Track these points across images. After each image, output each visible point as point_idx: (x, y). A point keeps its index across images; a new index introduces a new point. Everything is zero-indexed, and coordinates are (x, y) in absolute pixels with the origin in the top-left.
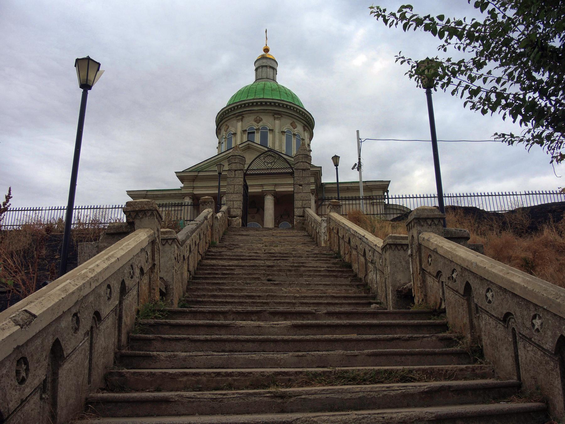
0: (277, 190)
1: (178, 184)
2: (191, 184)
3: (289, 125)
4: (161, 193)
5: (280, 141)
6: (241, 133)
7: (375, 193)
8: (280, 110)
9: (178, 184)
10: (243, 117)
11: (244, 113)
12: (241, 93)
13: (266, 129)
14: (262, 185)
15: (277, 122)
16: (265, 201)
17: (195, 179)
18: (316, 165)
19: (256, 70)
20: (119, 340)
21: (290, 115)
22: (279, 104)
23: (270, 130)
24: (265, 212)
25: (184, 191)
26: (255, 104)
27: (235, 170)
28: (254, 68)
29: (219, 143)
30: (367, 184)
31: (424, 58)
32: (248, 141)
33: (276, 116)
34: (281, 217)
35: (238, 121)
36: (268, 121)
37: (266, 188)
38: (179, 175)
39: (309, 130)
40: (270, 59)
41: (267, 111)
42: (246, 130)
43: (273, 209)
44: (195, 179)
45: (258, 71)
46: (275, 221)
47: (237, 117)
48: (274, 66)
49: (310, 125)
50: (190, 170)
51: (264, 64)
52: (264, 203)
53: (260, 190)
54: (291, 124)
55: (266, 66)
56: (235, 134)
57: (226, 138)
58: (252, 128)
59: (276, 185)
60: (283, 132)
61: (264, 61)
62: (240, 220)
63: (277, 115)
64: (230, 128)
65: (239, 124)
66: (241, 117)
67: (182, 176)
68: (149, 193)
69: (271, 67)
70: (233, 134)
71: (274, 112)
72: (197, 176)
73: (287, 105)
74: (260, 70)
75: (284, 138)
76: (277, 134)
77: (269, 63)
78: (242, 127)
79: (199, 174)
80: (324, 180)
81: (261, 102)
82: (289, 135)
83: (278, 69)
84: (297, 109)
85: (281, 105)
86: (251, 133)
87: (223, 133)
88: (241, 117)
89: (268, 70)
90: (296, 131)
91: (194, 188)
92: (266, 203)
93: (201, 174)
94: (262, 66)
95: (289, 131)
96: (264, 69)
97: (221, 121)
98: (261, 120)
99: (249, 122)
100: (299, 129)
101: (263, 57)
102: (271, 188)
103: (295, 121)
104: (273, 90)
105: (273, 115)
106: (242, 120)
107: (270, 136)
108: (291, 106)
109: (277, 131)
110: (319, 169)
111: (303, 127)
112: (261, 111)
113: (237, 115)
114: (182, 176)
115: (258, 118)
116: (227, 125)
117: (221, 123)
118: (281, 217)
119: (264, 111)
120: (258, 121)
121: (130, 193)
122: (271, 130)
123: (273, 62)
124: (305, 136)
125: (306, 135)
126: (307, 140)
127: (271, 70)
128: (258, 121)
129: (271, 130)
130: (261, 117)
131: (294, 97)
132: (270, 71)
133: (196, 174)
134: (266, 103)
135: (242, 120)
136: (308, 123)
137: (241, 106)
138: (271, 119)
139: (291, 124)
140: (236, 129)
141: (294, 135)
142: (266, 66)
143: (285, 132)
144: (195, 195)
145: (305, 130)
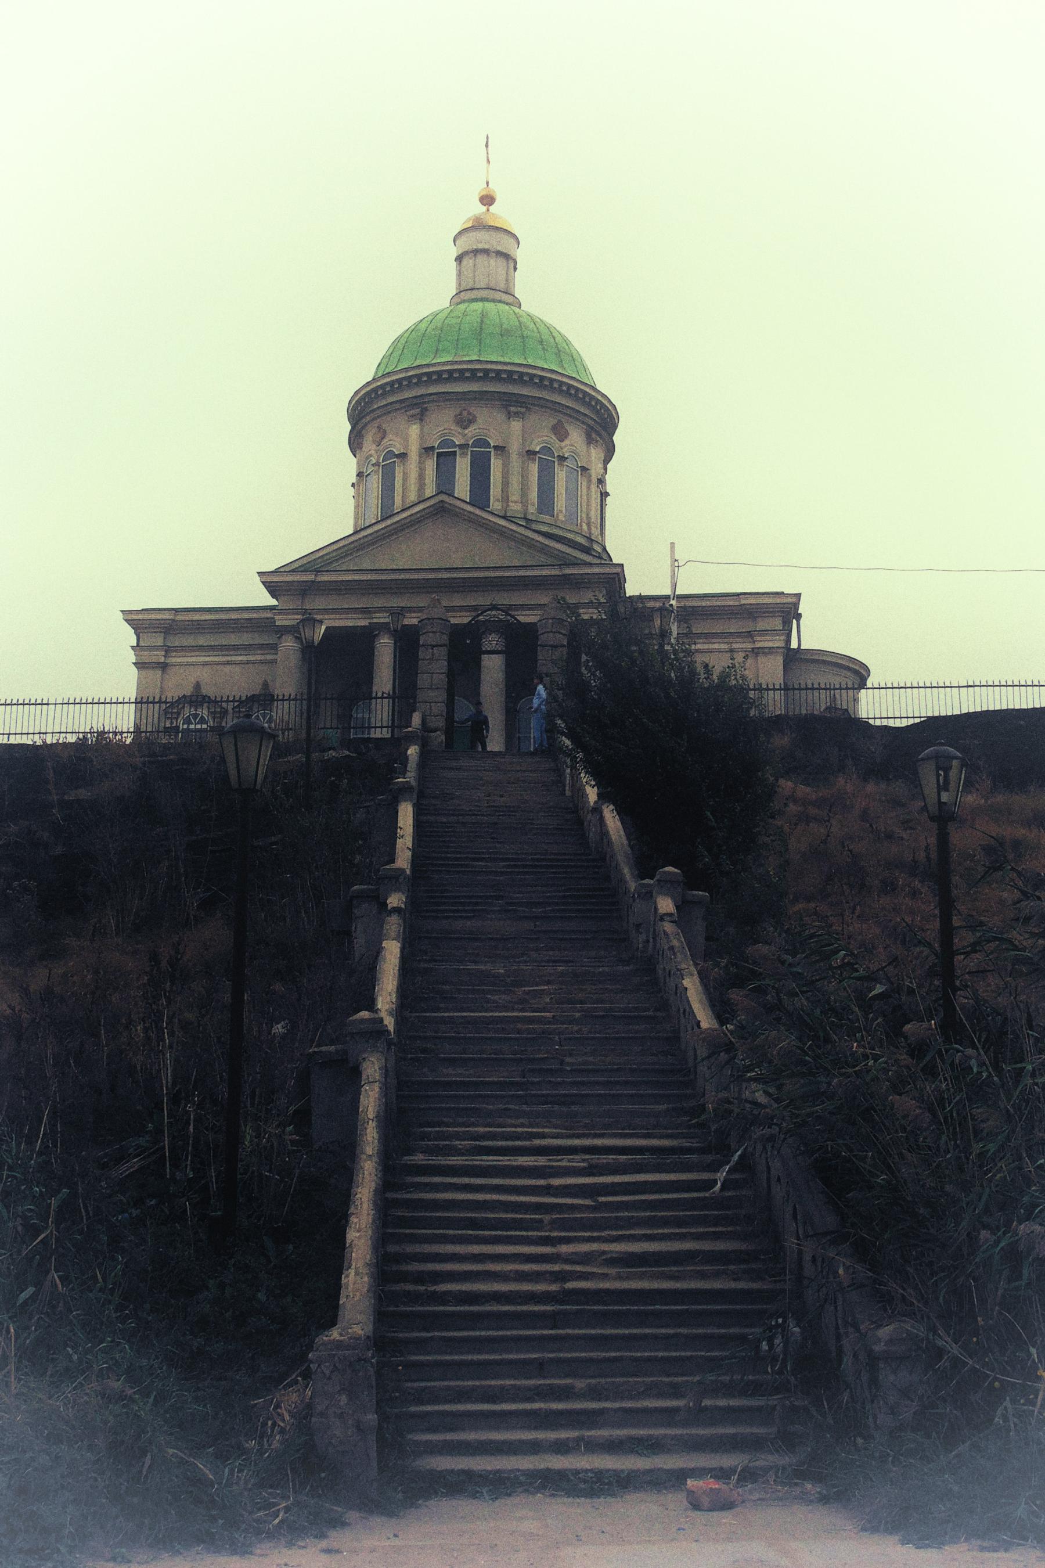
1: (267, 600)
4: (212, 617)
5: (524, 476)
6: (420, 456)
9: (267, 600)
10: (426, 409)
13: (488, 445)
15: (516, 425)
19: (459, 259)
23: (496, 448)
25: (281, 621)
27: (434, 646)
28: (454, 252)
29: (359, 475)
31: (637, 594)
32: (442, 492)
33: (512, 409)
36: (490, 424)
39: (604, 440)
42: (432, 448)
44: (305, 590)
45: (465, 262)
46: (508, 696)
49: (605, 429)
50: (296, 565)
51: (480, 246)
55: (486, 251)
56: (403, 456)
57: (377, 464)
60: (531, 453)
62: (443, 737)
63: (514, 406)
65: (414, 430)
66: (419, 409)
67: (273, 583)
68: (180, 617)
69: (499, 254)
70: (399, 456)
74: (468, 262)
76: (514, 456)
78: (422, 437)
79: (319, 579)
83: (521, 255)
84: (570, 386)
86: (445, 459)
87: (369, 445)
89: (492, 262)
90: (565, 448)
93: (325, 578)
94: (476, 252)
96: (481, 259)
99: (441, 425)
100: (576, 437)
101: (478, 225)
104: (505, 333)
105: (506, 407)
106: (421, 417)
107: (496, 465)
110: (618, 570)
114: (273, 583)
115: (465, 413)
120: (464, 422)
126: (596, 469)
127: (501, 262)
131: (561, 349)
132: (496, 265)
133: (311, 577)
134: (486, 372)
138: (500, 416)
140: (406, 439)
141: (562, 459)
142: (486, 252)
143: (535, 453)
145: (590, 440)
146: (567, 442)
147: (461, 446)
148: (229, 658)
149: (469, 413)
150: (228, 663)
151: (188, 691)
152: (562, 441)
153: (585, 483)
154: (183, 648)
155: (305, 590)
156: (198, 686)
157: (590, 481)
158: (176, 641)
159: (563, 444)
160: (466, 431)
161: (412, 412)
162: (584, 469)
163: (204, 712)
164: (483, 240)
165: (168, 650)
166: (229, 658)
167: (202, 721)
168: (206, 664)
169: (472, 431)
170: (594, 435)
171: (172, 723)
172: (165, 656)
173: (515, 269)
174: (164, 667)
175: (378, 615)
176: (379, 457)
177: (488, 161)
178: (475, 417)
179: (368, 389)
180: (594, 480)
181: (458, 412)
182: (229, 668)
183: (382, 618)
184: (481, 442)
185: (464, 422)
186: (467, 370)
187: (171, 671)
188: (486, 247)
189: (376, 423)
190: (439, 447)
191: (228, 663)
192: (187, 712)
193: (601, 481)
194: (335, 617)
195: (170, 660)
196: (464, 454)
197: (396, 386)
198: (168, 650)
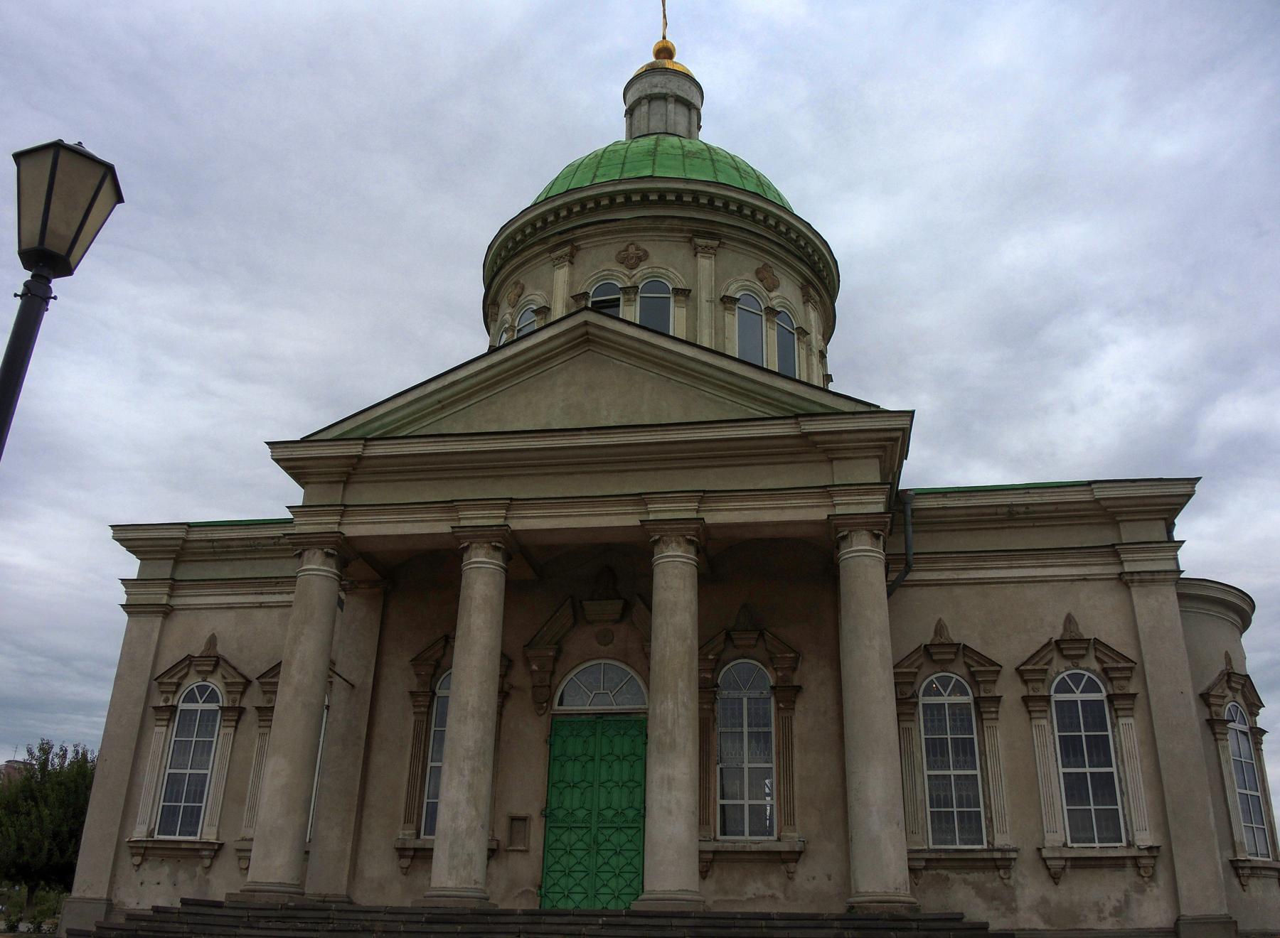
0: (711, 518)
2: (335, 495)
3: (749, 275)
7: (1130, 533)
8: (718, 219)
10: (578, 249)
11: (579, 233)
12: (574, 169)
14: (641, 499)
15: (705, 264)
16: (657, 571)
19: (630, 113)
21: (752, 239)
22: (712, 198)
23: (677, 292)
24: (657, 620)
25: (308, 526)
26: (620, 199)
30: (1099, 494)
33: (700, 241)
34: (728, 637)
35: (557, 263)
36: (668, 261)
37: (660, 511)
38: (286, 453)
39: (823, 303)
41: (667, 224)
42: (585, 295)
43: (694, 607)
45: (637, 113)
46: (702, 658)
47: (552, 250)
48: (696, 101)
51: (656, 91)
52: (649, 576)
53: (634, 521)
58: (611, 288)
59: (704, 496)
60: (728, 302)
61: (658, 79)
64: (527, 292)
65: (561, 276)
67: (294, 458)
69: (680, 100)
71: (694, 226)
72: (360, 458)
73: (741, 205)
77: (674, 86)
78: (571, 285)
81: (644, 194)
85: (719, 203)
88: (567, 249)
91: (344, 510)
92: (659, 580)
94: (651, 98)
98: (642, 257)
99: (599, 266)
100: (787, 293)
101: (650, 70)
102: (684, 510)
103: (770, 261)
104: (686, 155)
105: (690, 240)
106: (571, 259)
108: (755, 210)
111: (803, 288)
112: (644, 224)
114: (294, 458)
115: (632, 249)
116: (517, 283)
117: (498, 280)
118: (728, 637)
120: (632, 260)
121: (128, 536)
122: (683, 294)
123: (683, 81)
124: (807, 320)
125: (813, 319)
126: (816, 337)
127: (682, 110)
128: (632, 260)
129: (683, 294)
130: (644, 246)
132: (678, 116)
133: (355, 449)
134: (662, 194)
135: (571, 259)
137: (570, 211)
138: (680, 254)
139: (758, 272)
140: (550, 293)
141: (771, 312)
142: (663, 97)
144: (349, 540)
145: (807, 299)
147: (625, 290)
149: (638, 249)
151: (197, 649)
153: (803, 353)
155: (349, 474)
156: (212, 641)
159: (773, 294)
163: (215, 683)
164: (659, 84)
165: (174, 585)
167: (213, 697)
168: (230, 607)
169: (642, 270)
170: (812, 291)
171: (166, 700)
172: (170, 596)
173: (699, 128)
174: (167, 612)
178: (646, 254)
180: (816, 351)
182: (260, 614)
184: (655, 284)
186: (636, 191)
187: (180, 624)
190: (596, 294)
191: (261, 606)
192: (193, 682)
193: (823, 355)
195: (177, 602)
196: (629, 302)
198: (174, 585)
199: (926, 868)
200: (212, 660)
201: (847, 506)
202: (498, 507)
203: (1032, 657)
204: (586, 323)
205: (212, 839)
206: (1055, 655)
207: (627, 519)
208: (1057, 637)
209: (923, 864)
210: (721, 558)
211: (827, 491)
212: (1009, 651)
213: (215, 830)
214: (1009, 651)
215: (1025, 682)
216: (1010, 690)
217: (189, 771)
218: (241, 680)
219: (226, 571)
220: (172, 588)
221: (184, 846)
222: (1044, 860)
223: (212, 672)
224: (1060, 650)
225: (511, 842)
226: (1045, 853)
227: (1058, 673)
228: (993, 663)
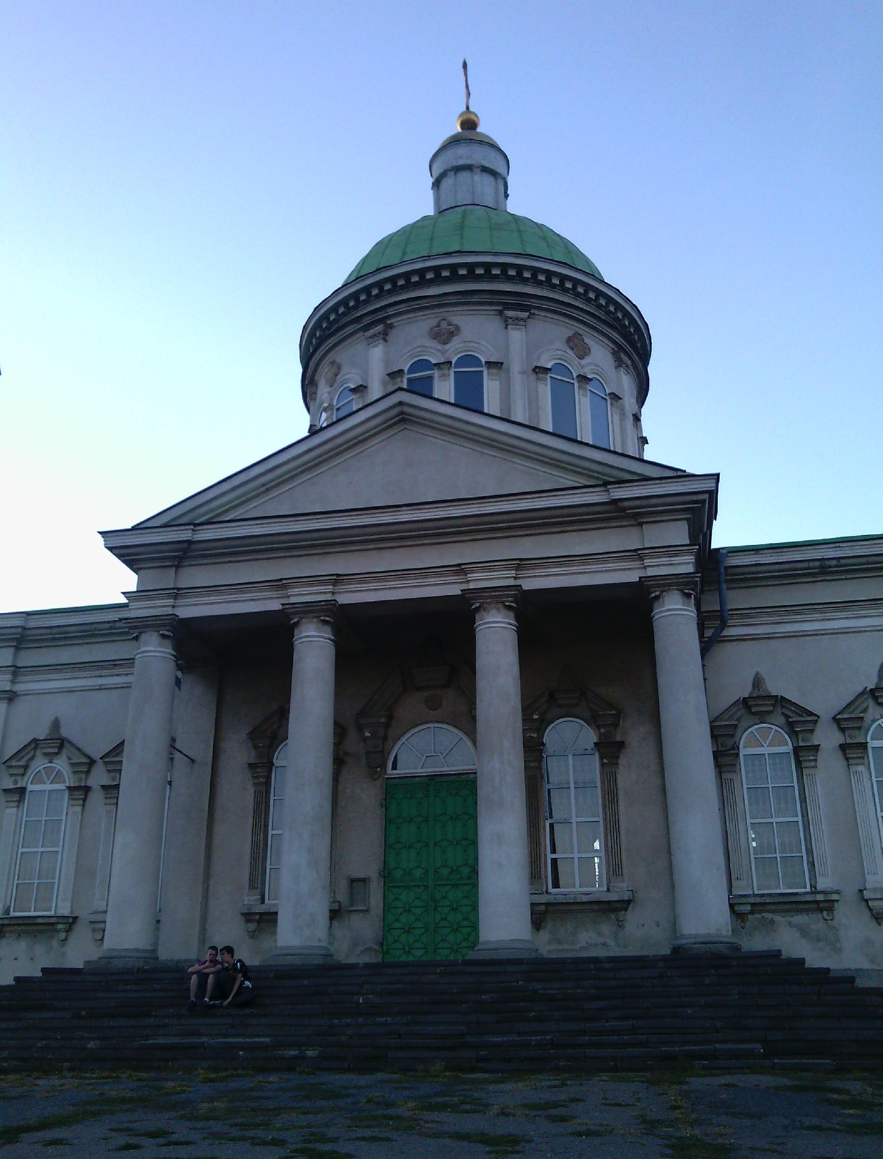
1: (111, 583)
2: (167, 579)
3: (561, 344)
10: (391, 326)
11: (391, 311)
15: (516, 336)
16: (479, 636)
17: (182, 555)
18: (690, 470)
19: (437, 184)
20: (633, 525)
23: (489, 364)
28: (430, 181)
33: (510, 313)
37: (479, 580)
38: (117, 542)
40: (481, 142)
42: (400, 372)
44: (182, 555)
46: (527, 711)
48: (501, 170)
51: (461, 162)
54: (569, 340)
60: (540, 371)
67: (126, 546)
68: (32, 624)
69: (485, 170)
70: (354, 390)
72: (189, 542)
75: (545, 391)
78: (387, 362)
80: (723, 536)
82: (565, 385)
83: (512, 180)
87: (323, 390)
88: (380, 328)
90: (587, 367)
94: (458, 169)
95: (561, 368)
96: (464, 176)
97: (316, 349)
99: (412, 340)
100: (600, 357)
103: (581, 329)
105: (501, 313)
109: (516, 366)
110: (709, 485)
111: (614, 354)
112: (453, 299)
113: (366, 321)
115: (444, 325)
116: (333, 363)
119: (465, 299)
120: (444, 335)
125: (626, 384)
127: (488, 179)
130: (456, 320)
132: (485, 186)
133: (186, 535)
136: (629, 338)
141: (583, 379)
142: (469, 168)
143: (547, 370)
145: (619, 363)
146: (586, 360)
148: (101, 681)
149: (450, 324)
150: (101, 688)
152: (581, 357)
153: (617, 418)
154: (36, 669)
156: (56, 725)
157: (623, 415)
158: (29, 658)
159: (583, 362)
160: (447, 347)
161: (372, 332)
162: (615, 397)
163: (61, 764)
165: (16, 671)
166: (101, 681)
175: (296, 590)
176: (332, 399)
177: (465, 65)
178: (458, 328)
179: (317, 316)
181: (434, 322)
182: (100, 696)
183: (301, 595)
185: (444, 335)
187: (22, 707)
188: (469, 162)
189: (326, 361)
190: (411, 371)
191: (101, 688)
192: (40, 764)
193: (637, 418)
194: (222, 595)
195: (18, 688)
197: (352, 304)
198: (16, 671)
199: (752, 912)
200: (57, 742)
201: (658, 568)
202: (507, 568)
203: (849, 705)
204: (401, 403)
205: (66, 912)
206: (871, 703)
207: (627, 574)
208: (871, 686)
209: (749, 908)
210: (545, 621)
211: (637, 555)
212: (824, 701)
213: (68, 904)
214: (824, 701)
215: (843, 730)
216: (827, 738)
217: (41, 849)
218: (84, 760)
219: (66, 655)
220: (15, 674)
221: (39, 921)
222: (866, 901)
223: (57, 754)
224: (875, 698)
225: (352, 902)
226: (867, 894)
227: (874, 721)
228: (810, 714)
